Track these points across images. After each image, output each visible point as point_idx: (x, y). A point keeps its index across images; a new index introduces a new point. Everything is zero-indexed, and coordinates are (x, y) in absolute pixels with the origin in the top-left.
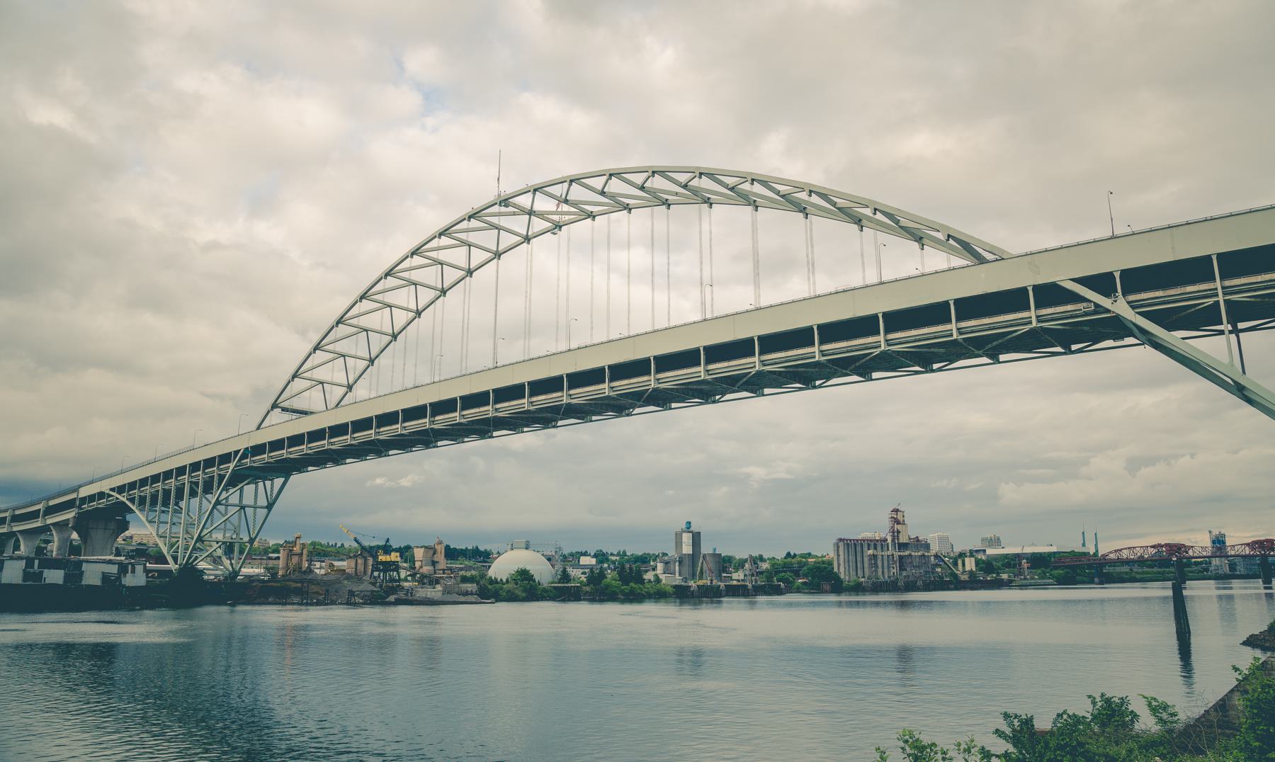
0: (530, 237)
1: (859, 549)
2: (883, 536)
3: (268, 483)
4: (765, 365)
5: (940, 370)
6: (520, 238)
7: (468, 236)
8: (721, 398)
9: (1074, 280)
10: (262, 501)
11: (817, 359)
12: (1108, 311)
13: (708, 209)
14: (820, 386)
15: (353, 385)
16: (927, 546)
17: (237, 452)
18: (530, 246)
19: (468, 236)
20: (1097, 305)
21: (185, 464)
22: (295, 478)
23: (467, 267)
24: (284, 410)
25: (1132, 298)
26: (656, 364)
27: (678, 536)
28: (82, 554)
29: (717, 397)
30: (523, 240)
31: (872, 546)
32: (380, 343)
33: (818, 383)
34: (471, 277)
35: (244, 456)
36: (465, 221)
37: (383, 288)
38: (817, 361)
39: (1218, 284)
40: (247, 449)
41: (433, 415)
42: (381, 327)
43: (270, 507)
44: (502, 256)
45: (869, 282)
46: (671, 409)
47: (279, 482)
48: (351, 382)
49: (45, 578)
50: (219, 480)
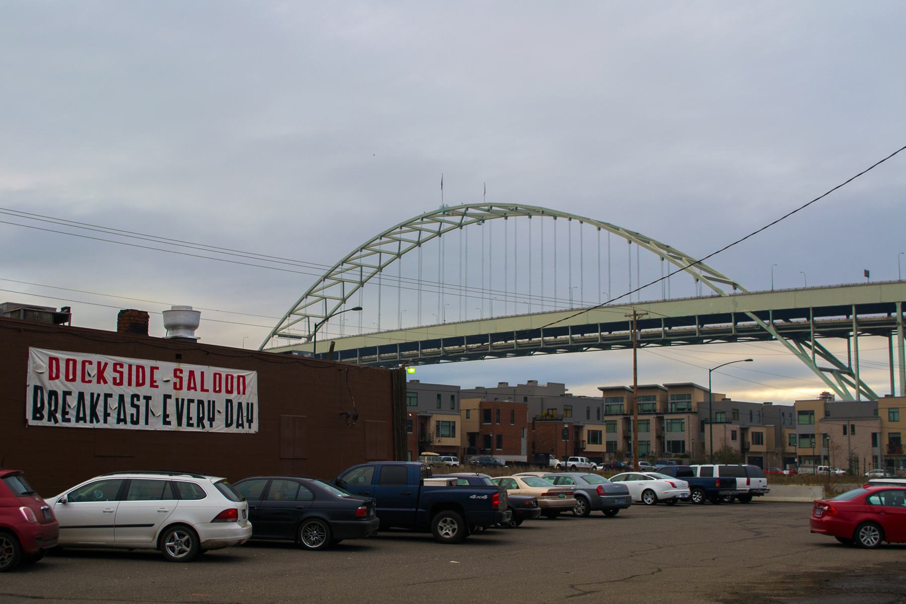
0: (441, 232)
2: (753, 446)
4: (495, 349)
5: (707, 343)
6: (376, 269)
7: (380, 247)
8: (534, 353)
13: (529, 219)
14: (585, 351)
18: (420, 248)
19: (380, 247)
20: (761, 327)
23: (342, 297)
29: (532, 352)
30: (378, 270)
32: (322, 329)
33: (584, 349)
36: (359, 252)
37: (287, 324)
38: (378, 362)
41: (361, 356)
44: (383, 269)
45: (485, 317)
49: (764, 486)
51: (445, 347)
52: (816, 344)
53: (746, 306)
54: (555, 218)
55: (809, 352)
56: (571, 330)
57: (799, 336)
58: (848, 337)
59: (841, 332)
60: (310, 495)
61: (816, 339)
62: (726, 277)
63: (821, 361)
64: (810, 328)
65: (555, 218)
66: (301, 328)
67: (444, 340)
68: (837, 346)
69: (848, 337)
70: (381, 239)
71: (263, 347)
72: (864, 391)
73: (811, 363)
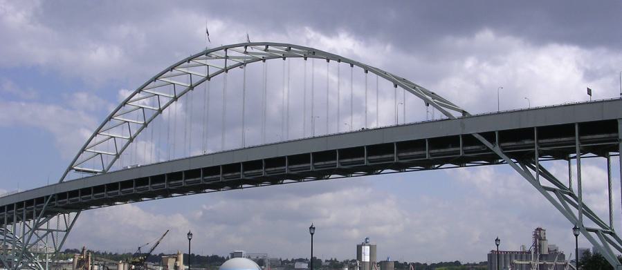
1: (508, 258)
3: (66, 215)
4: (292, 171)
9: (479, 134)
10: (63, 227)
11: (427, 158)
12: (491, 151)
14: (437, 168)
15: (121, 153)
16: (562, 256)
17: (48, 197)
20: (488, 148)
21: (12, 203)
22: (84, 213)
24: (77, 170)
25: (503, 145)
26: (203, 172)
27: (359, 248)
28: (524, 266)
31: (519, 257)
33: (436, 166)
34: (209, 80)
35: (53, 199)
39: (461, 149)
40: (54, 195)
42: (313, 61)
43: (68, 230)
46: (142, 201)
47: (73, 214)
48: (119, 149)
50: (37, 214)
51: (170, 181)
52: (540, 167)
53: (474, 130)
54: (352, 66)
55: (534, 173)
56: (339, 154)
57: (525, 159)
58: (569, 159)
59: (562, 154)
60: (460, 115)
61: (539, 162)
62: (456, 104)
63: (544, 182)
64: (534, 147)
65: (352, 66)
66: (109, 150)
67: (121, 182)
68: (557, 168)
69: (569, 159)
70: (189, 62)
71: (64, 177)
72: (568, 203)
73: (536, 183)
